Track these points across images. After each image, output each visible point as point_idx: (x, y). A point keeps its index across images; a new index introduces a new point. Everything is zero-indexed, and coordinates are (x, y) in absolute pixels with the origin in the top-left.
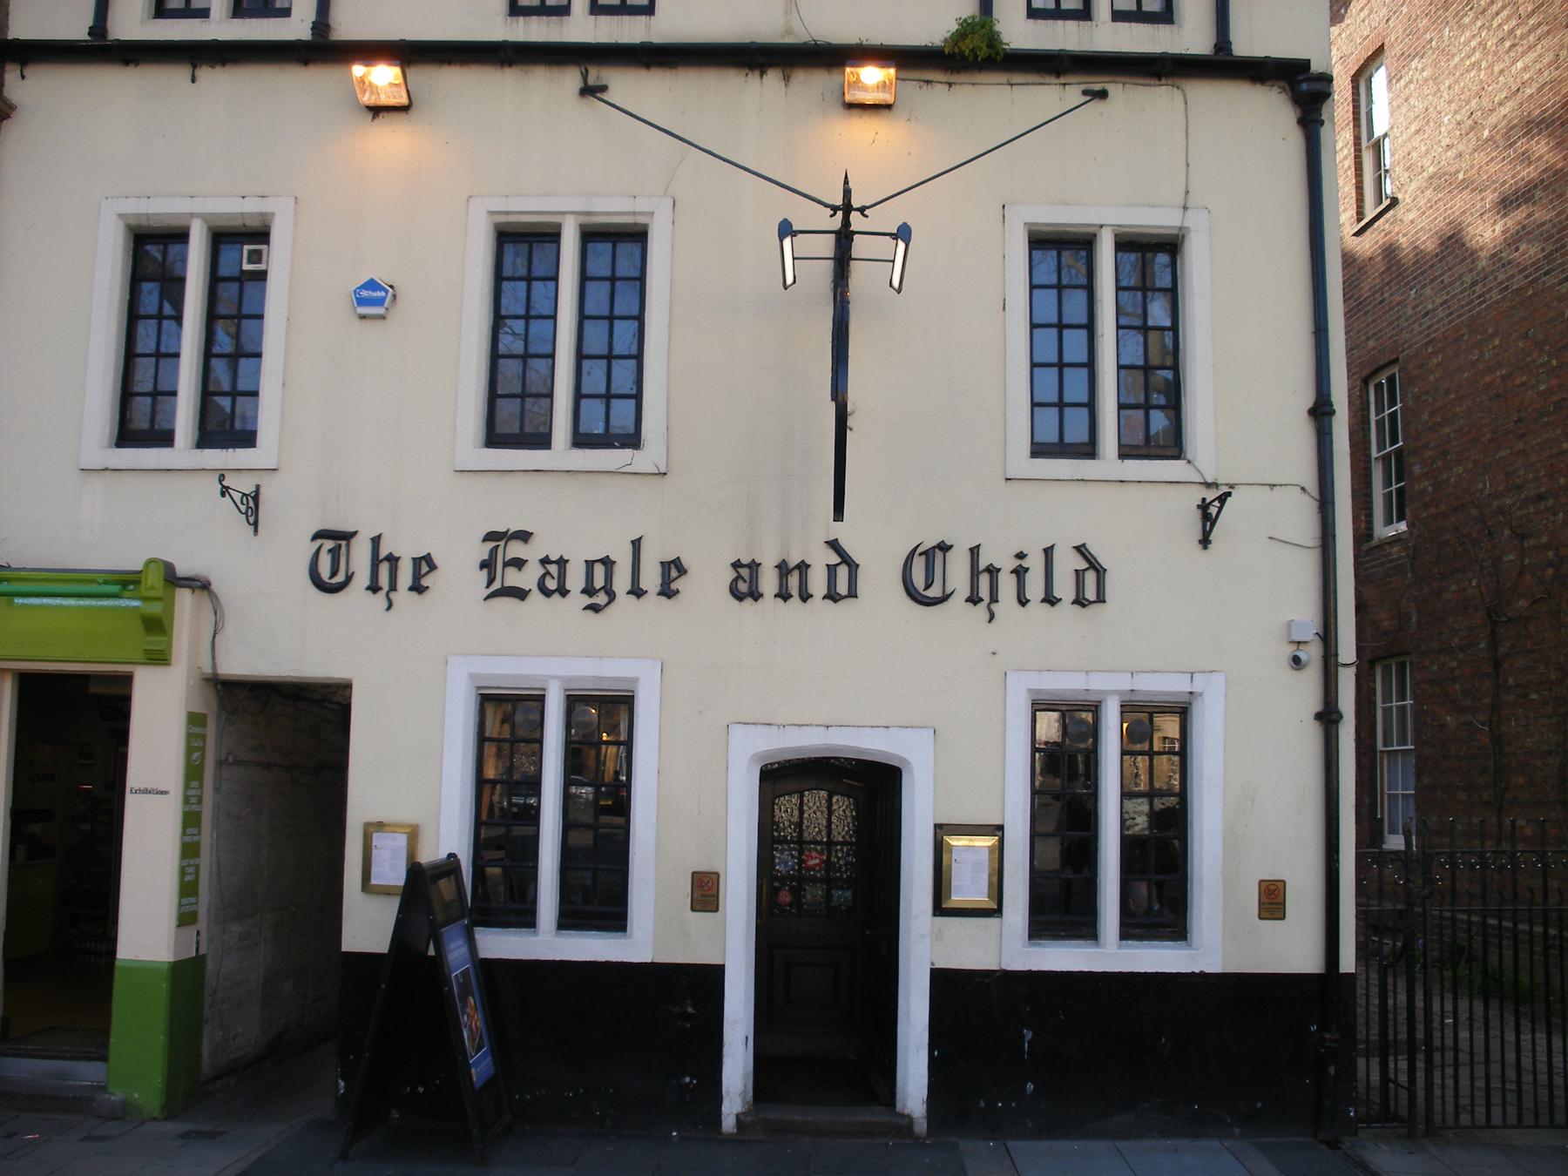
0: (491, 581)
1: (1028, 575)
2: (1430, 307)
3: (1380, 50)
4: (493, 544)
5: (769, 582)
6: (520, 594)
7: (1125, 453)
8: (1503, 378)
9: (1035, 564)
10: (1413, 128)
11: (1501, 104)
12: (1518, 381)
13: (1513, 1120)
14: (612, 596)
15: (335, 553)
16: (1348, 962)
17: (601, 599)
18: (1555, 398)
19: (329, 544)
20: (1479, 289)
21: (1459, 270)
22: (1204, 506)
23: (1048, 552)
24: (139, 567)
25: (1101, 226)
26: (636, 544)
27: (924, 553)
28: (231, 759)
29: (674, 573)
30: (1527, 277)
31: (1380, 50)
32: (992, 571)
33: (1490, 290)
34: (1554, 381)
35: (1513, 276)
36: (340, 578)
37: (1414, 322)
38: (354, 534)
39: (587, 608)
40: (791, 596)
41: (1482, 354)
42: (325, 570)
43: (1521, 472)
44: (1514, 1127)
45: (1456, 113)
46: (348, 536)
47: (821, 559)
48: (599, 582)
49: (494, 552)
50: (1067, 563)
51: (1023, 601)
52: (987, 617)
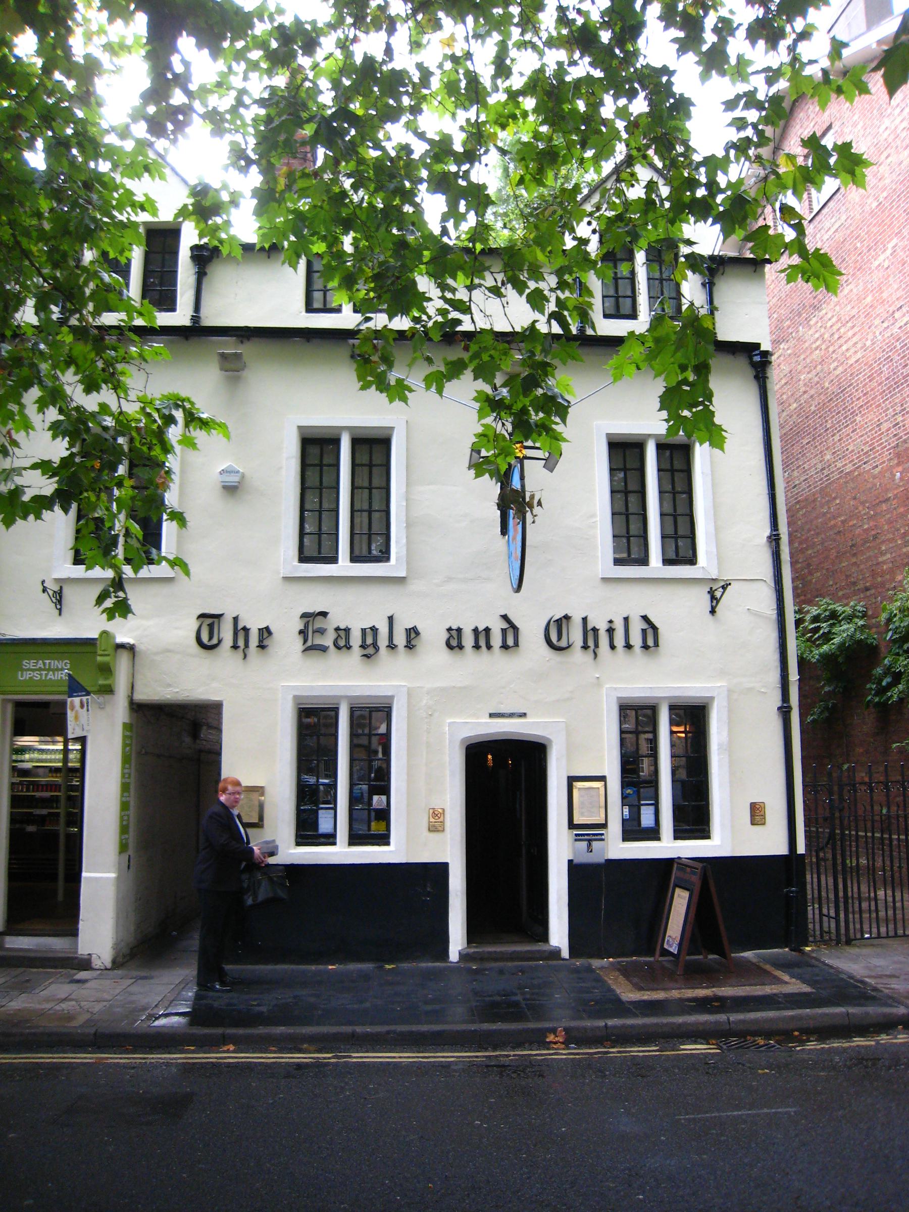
0: (305, 641)
2: (797, 482)
5: (468, 640)
6: (323, 649)
7: (667, 562)
8: (843, 522)
10: (783, 382)
11: (835, 369)
12: (851, 523)
13: (891, 933)
15: (211, 627)
16: (801, 849)
17: (371, 651)
18: (873, 533)
19: (209, 621)
20: (826, 472)
21: (814, 461)
22: (711, 592)
23: (626, 619)
24: (96, 636)
27: (557, 621)
29: (413, 635)
30: (854, 465)
32: (595, 630)
33: (833, 472)
34: (872, 524)
35: (846, 465)
38: (222, 615)
41: (829, 508)
42: (205, 638)
43: (855, 575)
45: (808, 373)
46: (219, 617)
47: (497, 626)
48: (369, 641)
49: (306, 626)
50: (637, 627)
51: (613, 647)
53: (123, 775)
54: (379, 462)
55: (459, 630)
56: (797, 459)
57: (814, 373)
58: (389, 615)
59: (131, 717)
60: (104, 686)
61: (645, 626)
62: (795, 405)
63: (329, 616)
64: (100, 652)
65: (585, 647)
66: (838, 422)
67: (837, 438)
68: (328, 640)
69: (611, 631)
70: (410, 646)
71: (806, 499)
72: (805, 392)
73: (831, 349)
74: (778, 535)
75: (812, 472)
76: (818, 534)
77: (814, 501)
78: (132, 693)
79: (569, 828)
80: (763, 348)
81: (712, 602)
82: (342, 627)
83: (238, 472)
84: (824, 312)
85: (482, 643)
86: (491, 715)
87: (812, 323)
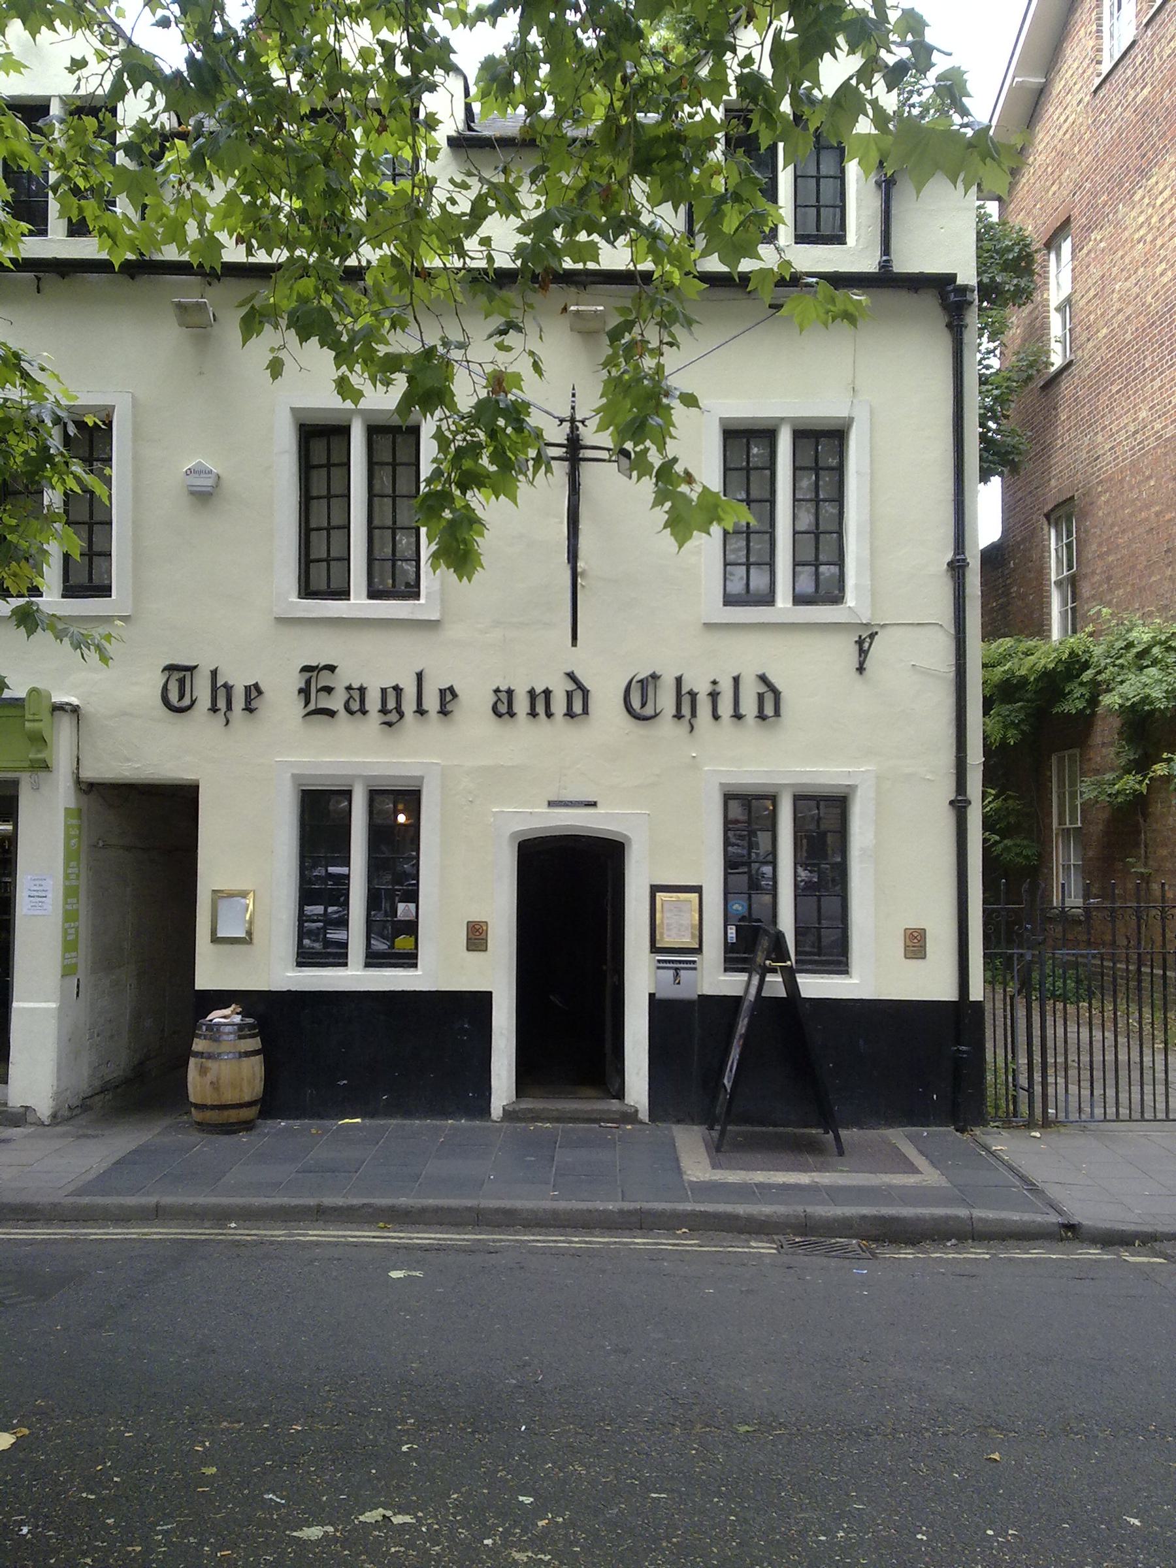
0: (307, 703)
1: (719, 697)
3: (1067, 222)
4: (307, 675)
5: (521, 705)
6: (331, 713)
7: (799, 600)
8: (1157, 514)
9: (726, 688)
10: (1092, 293)
11: (1162, 275)
14: (401, 715)
15: (182, 682)
16: (976, 993)
17: (393, 717)
19: (177, 675)
22: (860, 642)
23: (736, 680)
25: (782, 419)
26: (420, 676)
27: (641, 681)
28: (101, 844)
31: (1067, 222)
33: (1147, 438)
36: (186, 702)
37: (1088, 465)
38: (196, 667)
39: (385, 723)
40: (538, 714)
42: (174, 697)
44: (1114, 1121)
45: (1126, 280)
46: (191, 669)
48: (391, 704)
49: (308, 682)
51: (716, 717)
52: (689, 729)
53: (67, 876)
54: (338, 492)
55: (510, 692)
56: (1102, 417)
57: (1133, 280)
58: (418, 670)
59: (77, 799)
60: (38, 760)
61: (763, 689)
62: (1105, 331)
63: (337, 670)
64: (28, 716)
65: (678, 716)
66: (1160, 360)
67: (1157, 383)
68: (336, 702)
69: (714, 696)
70: (444, 712)
71: (1110, 479)
72: (1119, 311)
73: (1159, 242)
74: (964, 560)
75: (1122, 435)
76: (1124, 531)
77: (1121, 481)
78: (78, 769)
79: (652, 952)
80: (959, 281)
81: (860, 656)
82: (356, 685)
83: (210, 472)
84: (1153, 180)
85: (541, 709)
86: (551, 804)
87: (1137, 198)
